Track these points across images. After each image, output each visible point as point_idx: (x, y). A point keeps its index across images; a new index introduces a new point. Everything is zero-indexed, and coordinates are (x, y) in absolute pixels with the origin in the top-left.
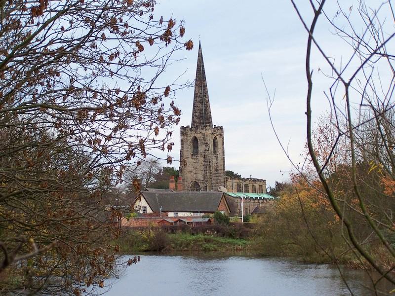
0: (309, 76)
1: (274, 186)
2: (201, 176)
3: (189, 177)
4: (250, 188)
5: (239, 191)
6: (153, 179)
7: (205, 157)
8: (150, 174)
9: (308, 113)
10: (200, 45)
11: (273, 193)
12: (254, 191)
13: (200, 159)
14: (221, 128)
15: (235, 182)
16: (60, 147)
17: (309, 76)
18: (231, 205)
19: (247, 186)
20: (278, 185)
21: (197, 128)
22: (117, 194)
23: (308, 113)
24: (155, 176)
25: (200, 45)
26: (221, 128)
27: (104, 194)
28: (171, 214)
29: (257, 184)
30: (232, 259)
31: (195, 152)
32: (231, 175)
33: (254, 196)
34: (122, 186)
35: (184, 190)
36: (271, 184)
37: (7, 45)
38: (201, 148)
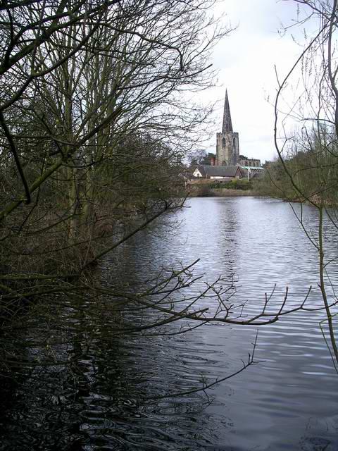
0: (276, 115)
1: (264, 163)
2: (227, 158)
3: (221, 159)
4: (252, 164)
5: (246, 165)
6: (202, 160)
7: (229, 148)
8: (201, 158)
9: (275, 130)
10: (227, 95)
11: (264, 166)
12: (254, 166)
13: (227, 149)
14: (237, 133)
15: (244, 161)
16: (157, 144)
17: (276, 115)
18: (243, 174)
19: (250, 163)
20: (267, 163)
21: (225, 133)
22: (184, 167)
23: (275, 130)
24: (204, 158)
25: (227, 95)
26: (237, 133)
27: (180, 168)
28: (212, 178)
29: (255, 162)
30: (162, 255)
31: (224, 147)
32: (242, 157)
33: (254, 168)
34: (186, 162)
35: (219, 166)
36: (263, 162)
37: (144, 108)
38: (227, 144)
